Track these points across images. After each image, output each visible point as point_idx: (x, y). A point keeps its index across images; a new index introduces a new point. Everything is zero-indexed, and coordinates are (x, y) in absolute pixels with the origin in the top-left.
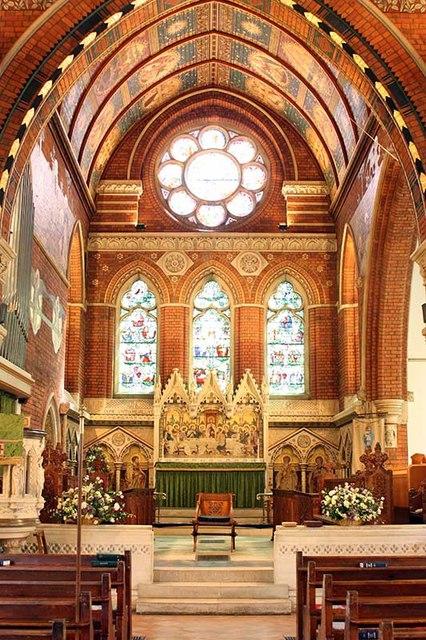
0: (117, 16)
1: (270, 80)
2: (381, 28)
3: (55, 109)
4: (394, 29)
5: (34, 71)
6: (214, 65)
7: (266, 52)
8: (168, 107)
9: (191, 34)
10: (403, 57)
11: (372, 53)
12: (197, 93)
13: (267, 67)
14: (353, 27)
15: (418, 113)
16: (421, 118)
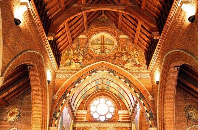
2: (137, 82)
4: (139, 82)
10: (142, 88)
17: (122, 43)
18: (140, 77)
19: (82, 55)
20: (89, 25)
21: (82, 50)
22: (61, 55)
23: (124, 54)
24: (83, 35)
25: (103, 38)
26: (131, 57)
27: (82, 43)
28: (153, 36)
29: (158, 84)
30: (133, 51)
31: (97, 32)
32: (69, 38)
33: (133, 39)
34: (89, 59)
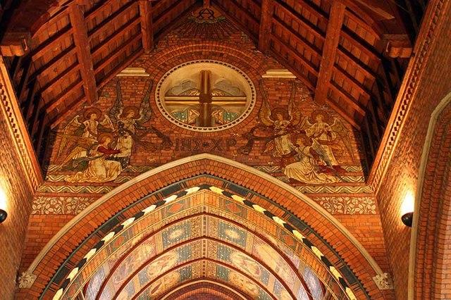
0: (131, 220)
1: (247, 273)
2: (331, 226)
3: (80, 290)
4: (341, 226)
5: (65, 260)
6: (204, 262)
7: (244, 251)
8: (169, 294)
9: (187, 239)
10: (350, 247)
11: (326, 245)
12: (192, 283)
13: (244, 263)
14: (310, 226)
15: (365, 289)
16: (367, 293)
17: (274, 95)
18: (343, 209)
19: (131, 133)
20: (157, 35)
21: (130, 116)
22: (55, 133)
23: (282, 132)
24: (136, 66)
25: (205, 78)
26: (308, 142)
27: (133, 94)
28: (389, 49)
29: (410, 225)
30: (313, 121)
31: (188, 58)
32: (89, 72)
33: (313, 81)
34: (155, 149)
